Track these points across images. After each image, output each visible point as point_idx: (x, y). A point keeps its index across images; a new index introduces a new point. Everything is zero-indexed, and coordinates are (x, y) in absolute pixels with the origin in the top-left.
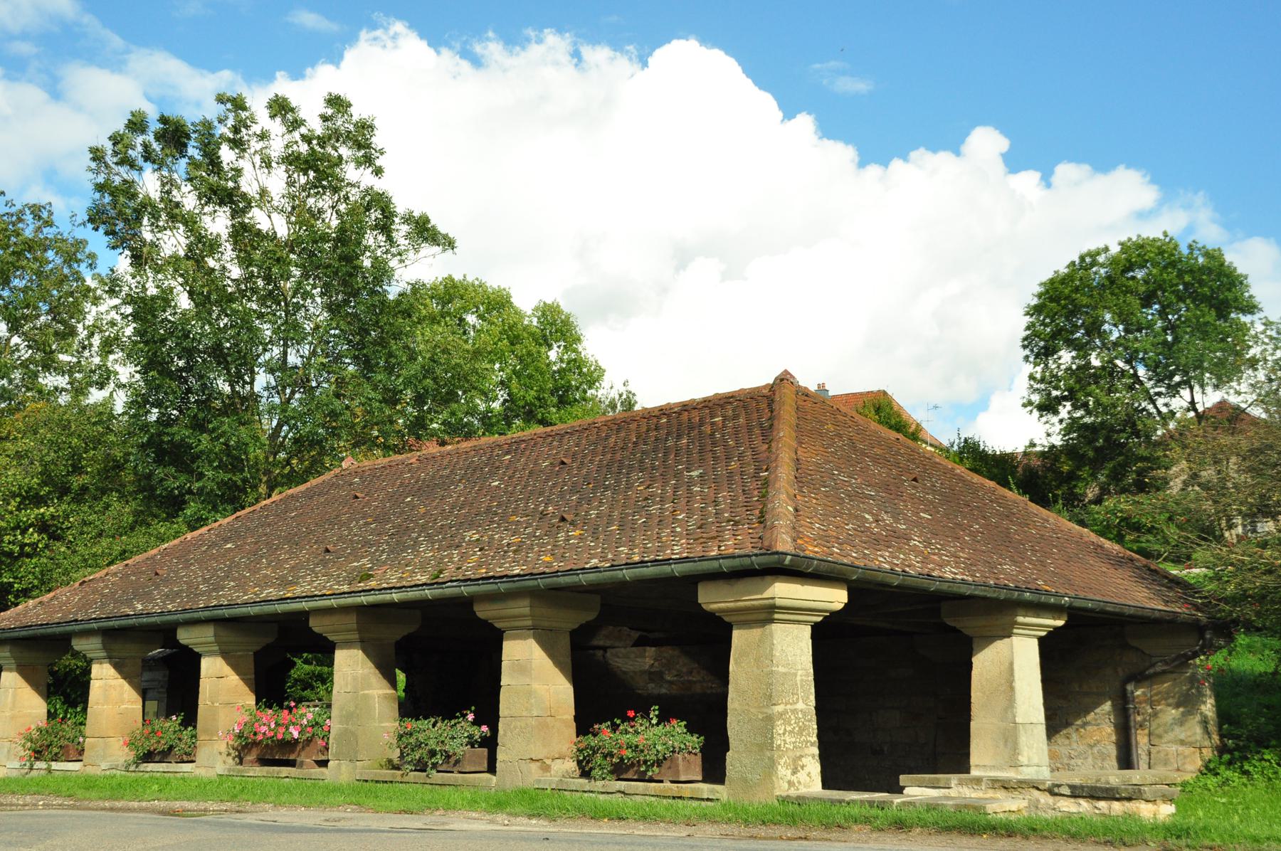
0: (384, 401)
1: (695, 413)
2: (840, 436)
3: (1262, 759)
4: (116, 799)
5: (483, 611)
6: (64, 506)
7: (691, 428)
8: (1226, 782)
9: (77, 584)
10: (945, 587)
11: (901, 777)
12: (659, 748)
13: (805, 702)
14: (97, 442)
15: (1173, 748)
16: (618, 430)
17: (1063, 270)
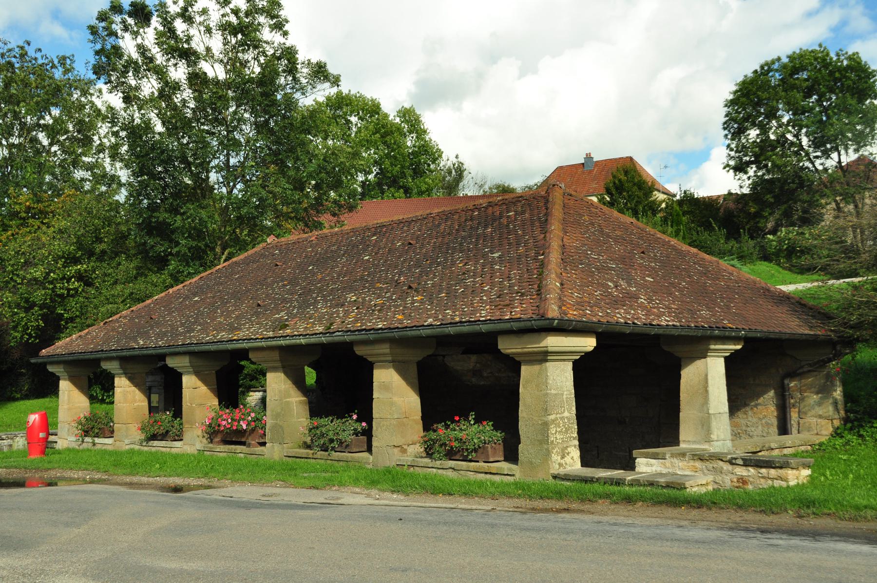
0: (295, 189)
1: (496, 208)
2: (592, 224)
3: (872, 427)
4: (134, 475)
5: (359, 351)
6: (92, 264)
7: (494, 220)
8: (847, 443)
9: (102, 324)
10: (661, 332)
11: (634, 452)
12: (476, 441)
13: (569, 412)
14: (108, 221)
15: (814, 420)
16: (446, 221)
17: (750, 75)
